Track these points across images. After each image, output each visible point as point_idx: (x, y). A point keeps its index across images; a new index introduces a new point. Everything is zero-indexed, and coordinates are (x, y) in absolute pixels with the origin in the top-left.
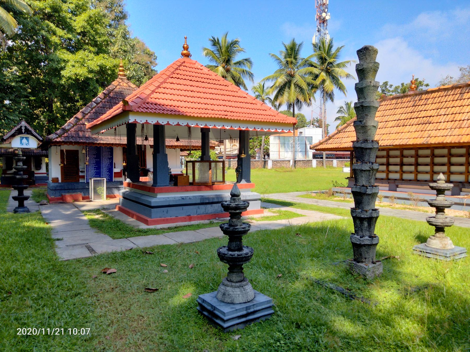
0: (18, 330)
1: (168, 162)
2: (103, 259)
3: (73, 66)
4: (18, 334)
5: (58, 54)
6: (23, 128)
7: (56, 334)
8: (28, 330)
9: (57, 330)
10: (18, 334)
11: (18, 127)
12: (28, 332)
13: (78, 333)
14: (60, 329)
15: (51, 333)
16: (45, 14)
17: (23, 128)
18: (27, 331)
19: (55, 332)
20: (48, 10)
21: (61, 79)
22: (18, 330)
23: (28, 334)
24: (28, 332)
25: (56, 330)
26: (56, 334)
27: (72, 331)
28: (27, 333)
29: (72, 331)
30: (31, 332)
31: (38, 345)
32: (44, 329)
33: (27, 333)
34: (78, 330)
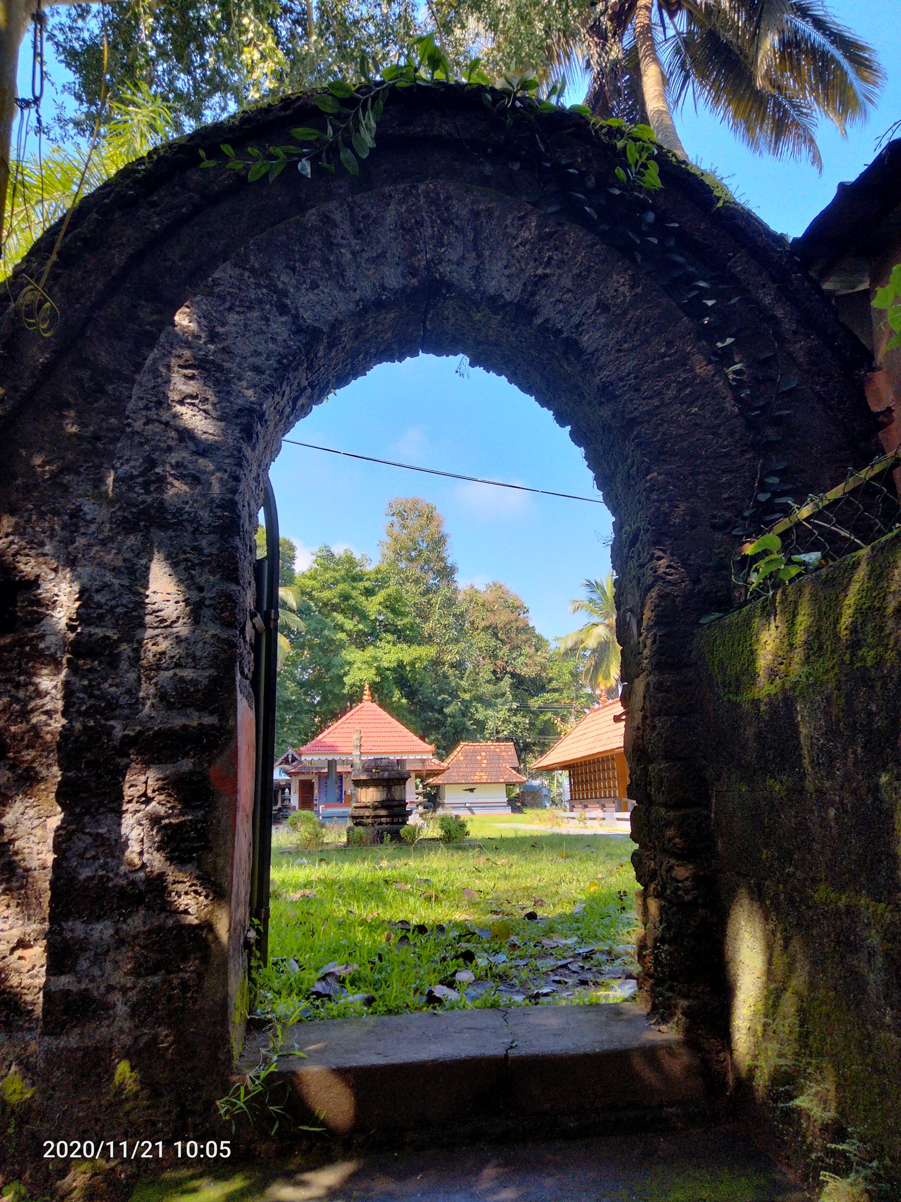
0: (45, 1144)
1: (347, 383)
2: (871, 910)
3: (360, 669)
4: (46, 1156)
5: (343, 655)
6: (290, 757)
7: (144, 1156)
8: (71, 1144)
9: (147, 1145)
10: (46, 1156)
11: (285, 755)
12: (71, 1150)
13: (198, 1155)
14: (153, 1144)
15: (129, 1155)
16: (333, 605)
17: (290, 757)
18: (69, 1147)
19: (140, 1152)
20: (336, 600)
21: (343, 688)
22: (45, 1144)
23: (72, 1156)
24: (71, 1150)
25: (143, 1144)
26: (144, 1156)
27: (184, 1149)
28: (70, 1152)
29: (184, 1149)
30: (80, 1152)
31: (521, 932)
32: (111, 1144)
33: (70, 1152)
34: (199, 1146)
